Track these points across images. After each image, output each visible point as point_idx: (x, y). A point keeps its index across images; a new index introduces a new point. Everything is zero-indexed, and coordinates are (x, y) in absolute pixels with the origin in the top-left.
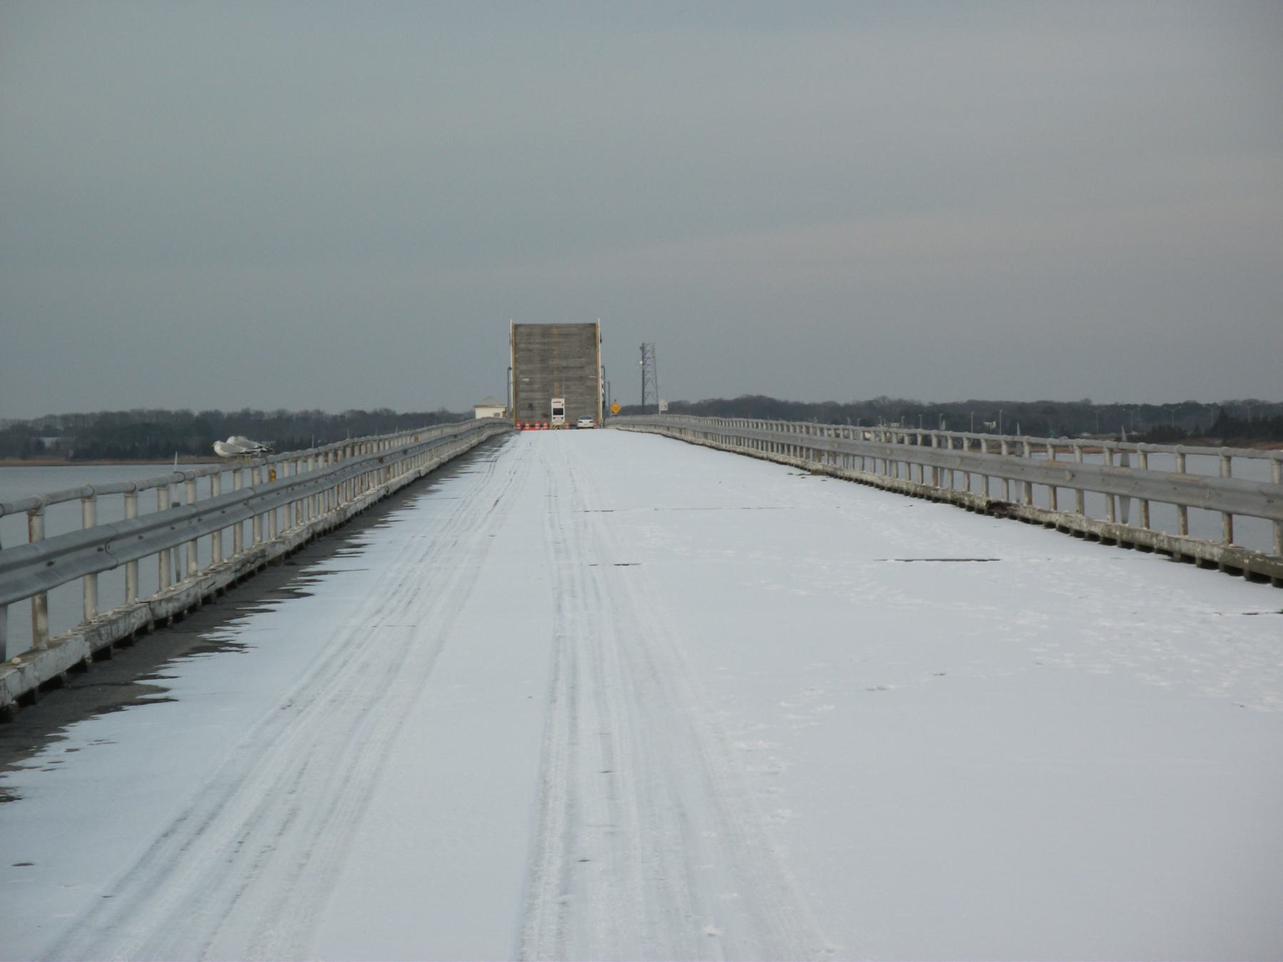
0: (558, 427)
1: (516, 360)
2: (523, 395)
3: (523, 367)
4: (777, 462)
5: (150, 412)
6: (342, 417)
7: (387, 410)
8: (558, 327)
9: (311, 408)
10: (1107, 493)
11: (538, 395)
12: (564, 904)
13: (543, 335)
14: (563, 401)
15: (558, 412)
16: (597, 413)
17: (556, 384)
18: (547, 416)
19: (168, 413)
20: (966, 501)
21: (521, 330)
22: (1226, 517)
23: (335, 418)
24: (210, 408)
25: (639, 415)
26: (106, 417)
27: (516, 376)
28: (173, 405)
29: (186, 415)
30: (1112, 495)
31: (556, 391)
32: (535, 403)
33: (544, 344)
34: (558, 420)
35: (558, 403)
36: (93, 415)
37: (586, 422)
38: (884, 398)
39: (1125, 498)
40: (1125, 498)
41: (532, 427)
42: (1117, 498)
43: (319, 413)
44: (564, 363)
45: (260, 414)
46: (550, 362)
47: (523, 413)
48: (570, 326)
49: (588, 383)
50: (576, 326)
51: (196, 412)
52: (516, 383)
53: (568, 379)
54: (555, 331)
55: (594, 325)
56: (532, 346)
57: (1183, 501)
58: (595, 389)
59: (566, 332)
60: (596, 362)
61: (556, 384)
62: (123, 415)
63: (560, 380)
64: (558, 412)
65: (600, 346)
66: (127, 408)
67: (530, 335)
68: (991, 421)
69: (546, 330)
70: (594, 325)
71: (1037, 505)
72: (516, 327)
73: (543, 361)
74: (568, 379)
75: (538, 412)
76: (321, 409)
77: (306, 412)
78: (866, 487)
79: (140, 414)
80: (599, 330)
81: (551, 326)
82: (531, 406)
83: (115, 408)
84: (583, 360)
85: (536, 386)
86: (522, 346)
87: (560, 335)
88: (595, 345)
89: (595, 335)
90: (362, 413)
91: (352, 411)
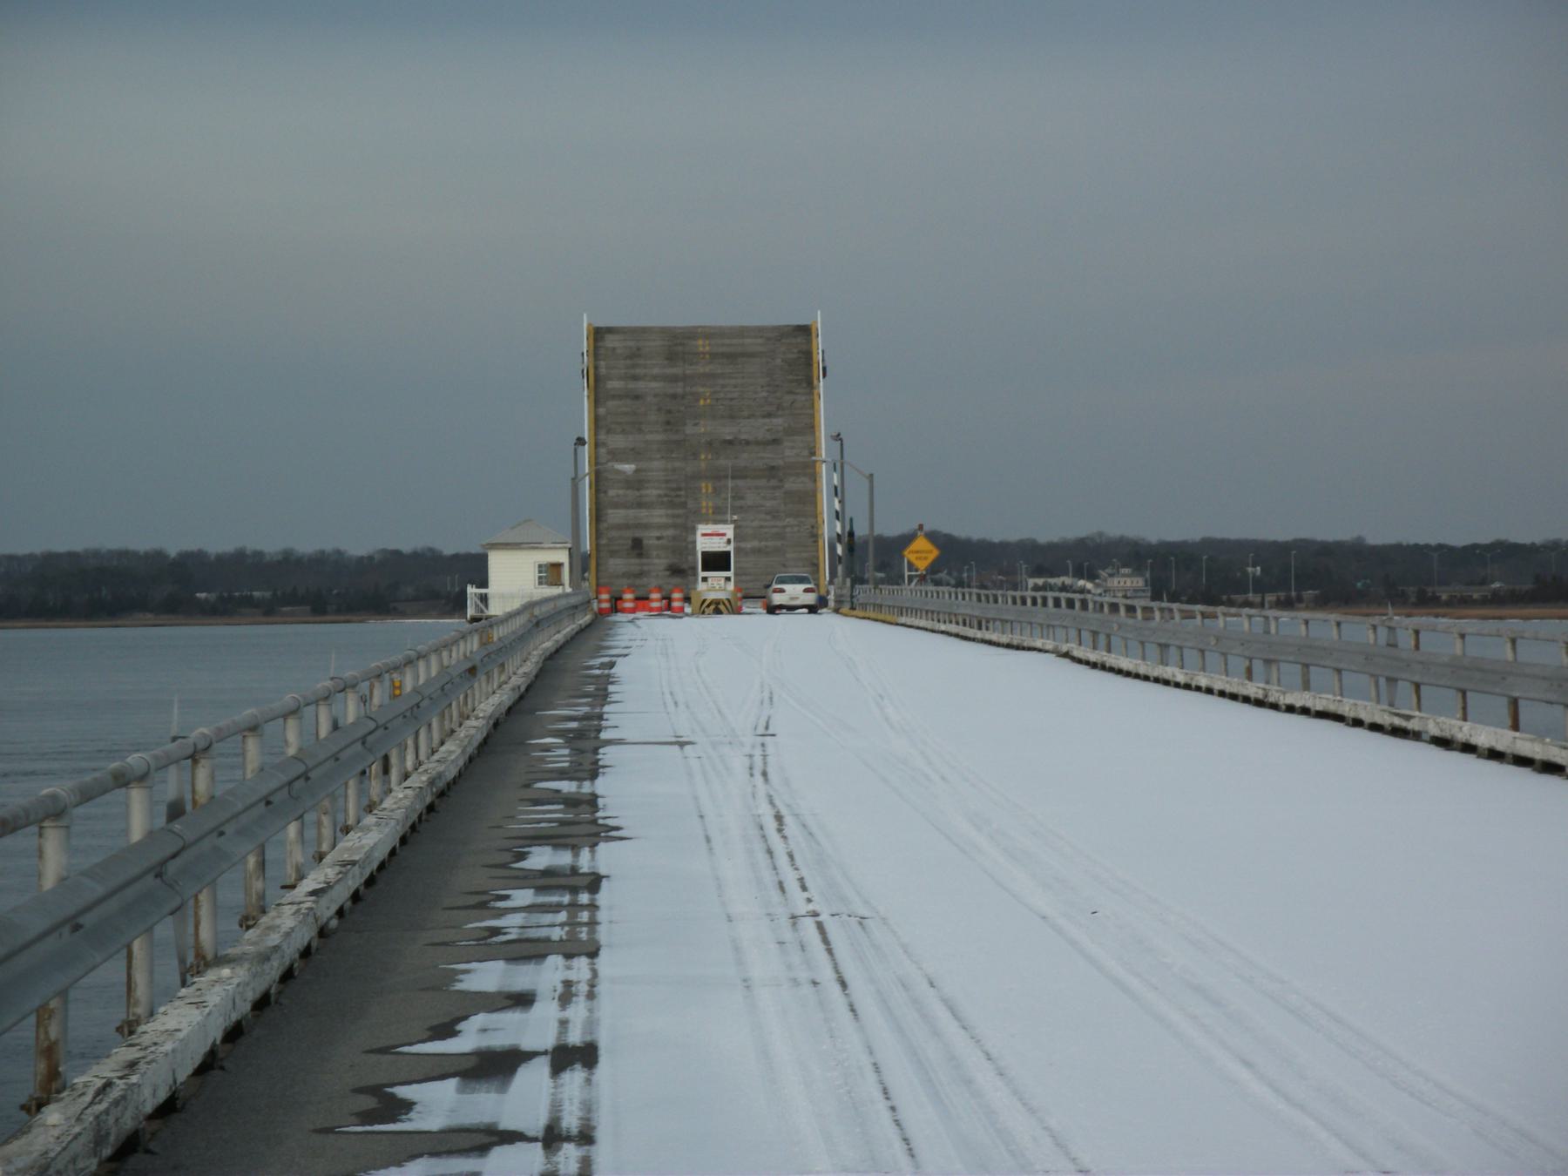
0: (717, 608)
1: (597, 421)
2: (615, 516)
3: (618, 441)
4: (1119, 672)
5: (110, 552)
6: (371, 558)
7: (431, 550)
8: (710, 334)
9: (328, 546)
10: (1372, 675)
11: (658, 516)
13: (672, 357)
14: (729, 530)
15: (717, 561)
16: (815, 566)
17: (706, 487)
18: (681, 571)
19: (135, 554)
20: (1193, 684)
21: (610, 341)
22: (1460, 695)
25: (868, 574)
26: (50, 559)
27: (596, 461)
28: (141, 543)
29: (159, 555)
30: (1375, 677)
31: (706, 504)
32: (650, 538)
33: (674, 379)
34: (715, 585)
35: (711, 537)
36: (31, 557)
37: (794, 592)
38: (1101, 534)
39: (1392, 681)
40: (1392, 681)
41: (642, 600)
42: (1382, 681)
43: (338, 552)
44: (727, 431)
45: (259, 554)
46: (689, 430)
47: (616, 564)
48: (742, 332)
49: (792, 484)
50: (759, 331)
51: (173, 551)
52: (600, 481)
53: (739, 474)
54: (701, 345)
55: (805, 331)
56: (641, 385)
57: (1464, 685)
58: (808, 499)
59: (730, 349)
60: (811, 428)
61: (706, 487)
62: (72, 556)
63: (717, 476)
64: (717, 561)
65: (822, 385)
66: (78, 547)
67: (635, 354)
69: (678, 344)
70: (805, 331)
71: (612, 561)
72: (598, 334)
74: (739, 474)
75: (658, 563)
76: (342, 548)
77: (323, 552)
78: (1129, 681)
79: (96, 554)
80: (819, 344)
81: (691, 334)
82: (637, 546)
83: (60, 545)
84: (778, 422)
85: (652, 493)
86: (614, 385)
87: (714, 356)
88: (810, 384)
89: (807, 356)
90: (397, 553)
91: (384, 551)
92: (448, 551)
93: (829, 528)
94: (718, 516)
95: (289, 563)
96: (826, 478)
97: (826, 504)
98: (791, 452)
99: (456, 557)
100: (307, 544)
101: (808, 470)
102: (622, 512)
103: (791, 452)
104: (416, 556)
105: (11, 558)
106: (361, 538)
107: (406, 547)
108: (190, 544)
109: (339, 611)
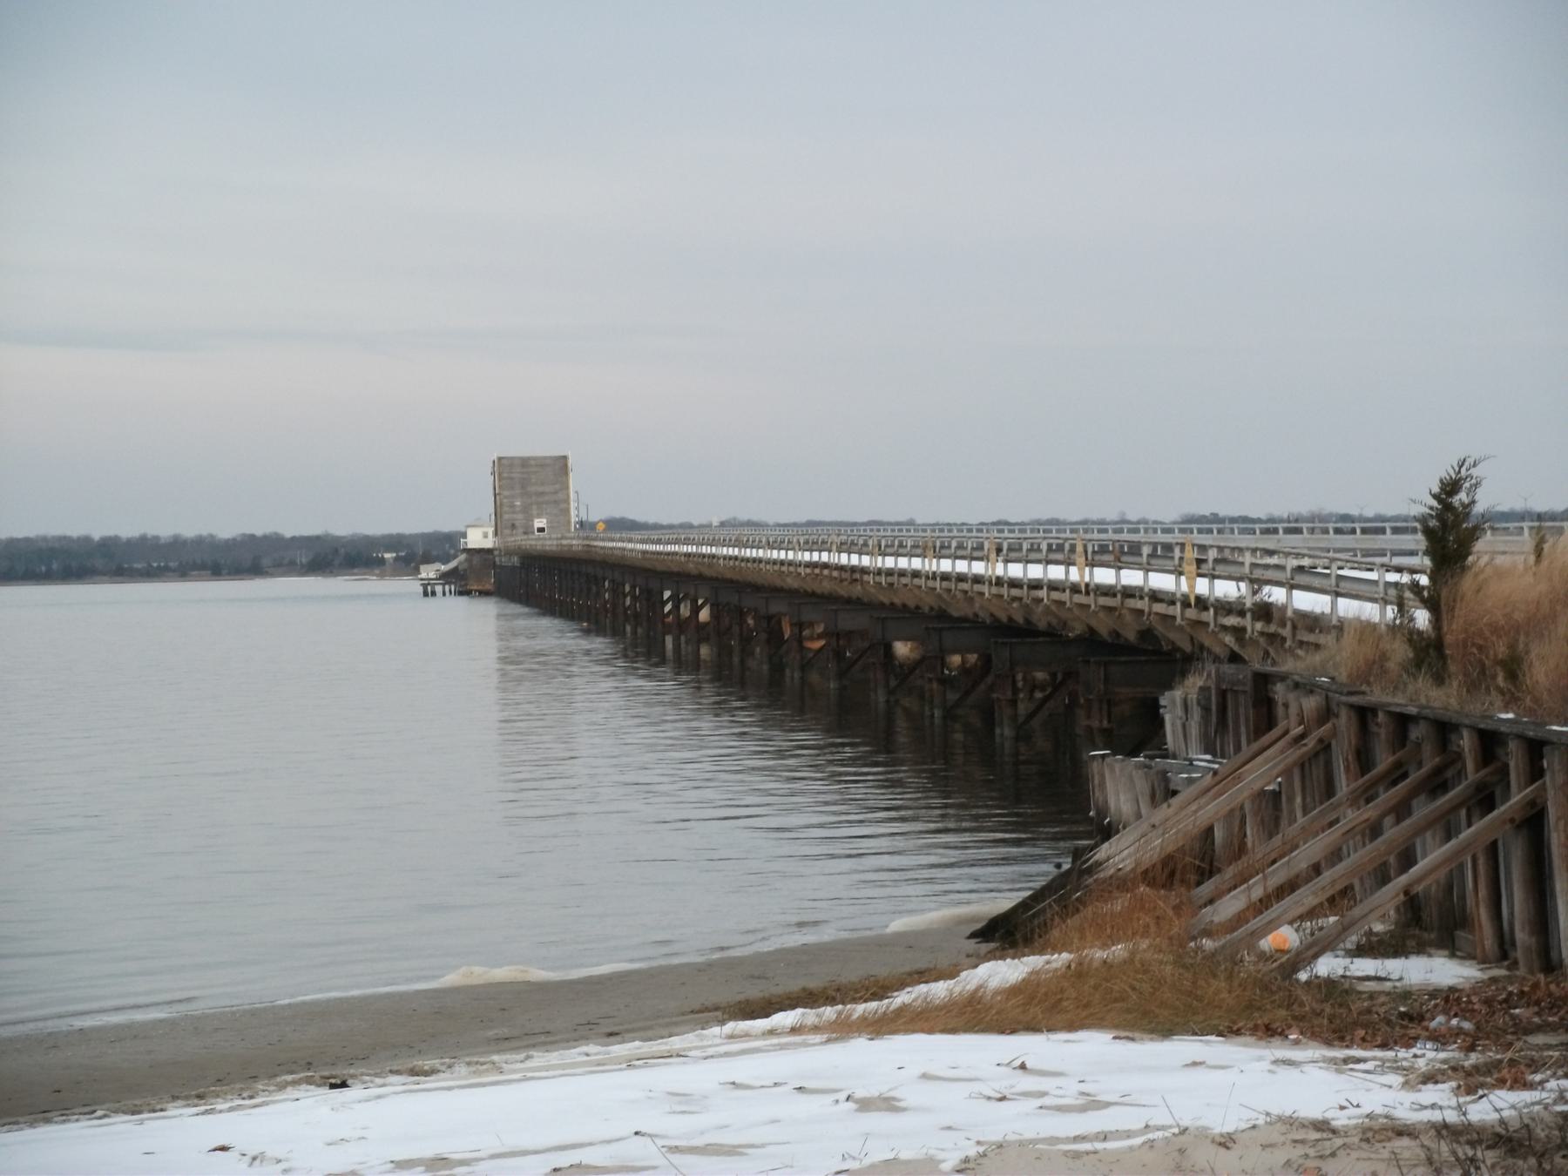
8: (535, 459)
11: (520, 516)
12: (999, 550)
23: (227, 541)
24: (110, 532)
28: (75, 530)
43: (212, 536)
44: (541, 489)
45: (157, 538)
55: (565, 458)
58: (567, 511)
59: (541, 463)
60: (567, 488)
62: (27, 540)
67: (511, 466)
68: (964, 669)
69: (525, 462)
70: (565, 458)
73: (523, 487)
74: (547, 503)
79: (45, 539)
81: (529, 459)
82: (513, 526)
83: (20, 533)
88: (566, 474)
89: (566, 466)
90: (253, 536)
91: (244, 535)
92: (288, 534)
93: (574, 519)
94: (539, 516)
95: (177, 544)
96: (573, 505)
97: (573, 512)
98: (561, 496)
99: (293, 539)
100: (189, 531)
101: (567, 501)
102: (1355, 603)
103: (561, 496)
104: (265, 537)
105: (12, 542)
106: (226, 527)
107: (259, 533)
108: (109, 532)
109: (229, 574)
